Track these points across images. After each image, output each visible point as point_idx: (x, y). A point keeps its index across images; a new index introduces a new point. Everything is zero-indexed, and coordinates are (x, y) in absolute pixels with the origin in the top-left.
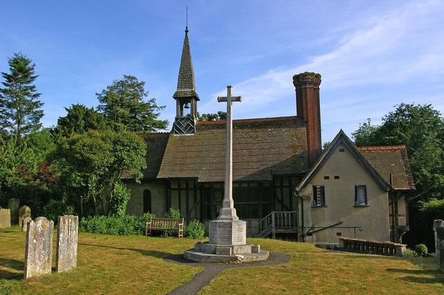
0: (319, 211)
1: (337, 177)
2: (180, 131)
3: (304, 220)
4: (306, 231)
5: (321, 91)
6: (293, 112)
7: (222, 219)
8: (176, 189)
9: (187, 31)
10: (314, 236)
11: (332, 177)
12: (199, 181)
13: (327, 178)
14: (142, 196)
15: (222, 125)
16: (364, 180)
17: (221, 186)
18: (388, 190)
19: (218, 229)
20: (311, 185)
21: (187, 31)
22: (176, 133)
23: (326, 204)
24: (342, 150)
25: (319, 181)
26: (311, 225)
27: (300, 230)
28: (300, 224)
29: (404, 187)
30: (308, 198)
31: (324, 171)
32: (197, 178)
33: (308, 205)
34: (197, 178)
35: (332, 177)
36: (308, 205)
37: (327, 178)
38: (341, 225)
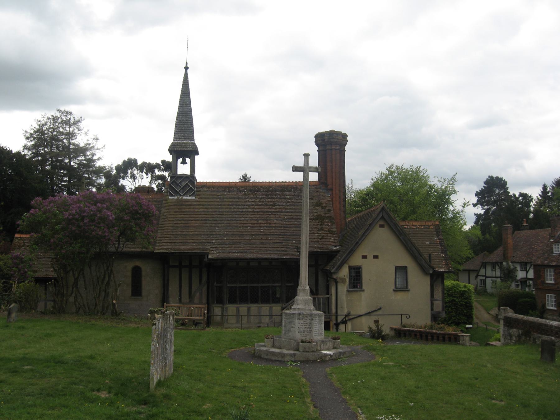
0: (355, 296)
1: (376, 257)
2: (177, 193)
3: (339, 306)
4: (340, 319)
5: (347, 154)
6: (197, 181)
7: (295, 309)
8: (494, 270)
9: (186, 68)
10: (349, 324)
11: (370, 257)
12: (210, 257)
13: (364, 257)
14: (129, 274)
15: (139, 192)
16: (405, 260)
17: (296, 263)
18: (431, 272)
19: (296, 321)
20: (347, 266)
21: (186, 68)
22: (172, 195)
23: (409, 287)
24: (382, 226)
25: (356, 260)
26: (345, 312)
27: (334, 317)
28: (334, 311)
29: (441, 268)
30: (343, 281)
31: (363, 250)
32: (207, 254)
33: (343, 289)
34: (207, 254)
35: (370, 257)
36: (343, 289)
37: (364, 257)
38: (380, 312)
